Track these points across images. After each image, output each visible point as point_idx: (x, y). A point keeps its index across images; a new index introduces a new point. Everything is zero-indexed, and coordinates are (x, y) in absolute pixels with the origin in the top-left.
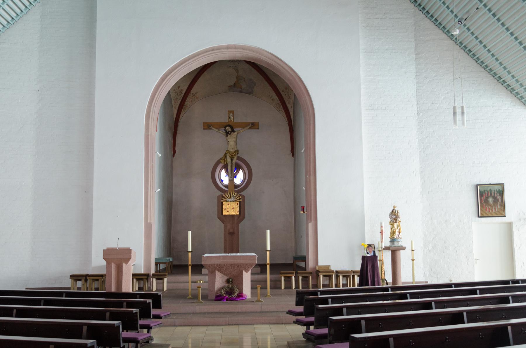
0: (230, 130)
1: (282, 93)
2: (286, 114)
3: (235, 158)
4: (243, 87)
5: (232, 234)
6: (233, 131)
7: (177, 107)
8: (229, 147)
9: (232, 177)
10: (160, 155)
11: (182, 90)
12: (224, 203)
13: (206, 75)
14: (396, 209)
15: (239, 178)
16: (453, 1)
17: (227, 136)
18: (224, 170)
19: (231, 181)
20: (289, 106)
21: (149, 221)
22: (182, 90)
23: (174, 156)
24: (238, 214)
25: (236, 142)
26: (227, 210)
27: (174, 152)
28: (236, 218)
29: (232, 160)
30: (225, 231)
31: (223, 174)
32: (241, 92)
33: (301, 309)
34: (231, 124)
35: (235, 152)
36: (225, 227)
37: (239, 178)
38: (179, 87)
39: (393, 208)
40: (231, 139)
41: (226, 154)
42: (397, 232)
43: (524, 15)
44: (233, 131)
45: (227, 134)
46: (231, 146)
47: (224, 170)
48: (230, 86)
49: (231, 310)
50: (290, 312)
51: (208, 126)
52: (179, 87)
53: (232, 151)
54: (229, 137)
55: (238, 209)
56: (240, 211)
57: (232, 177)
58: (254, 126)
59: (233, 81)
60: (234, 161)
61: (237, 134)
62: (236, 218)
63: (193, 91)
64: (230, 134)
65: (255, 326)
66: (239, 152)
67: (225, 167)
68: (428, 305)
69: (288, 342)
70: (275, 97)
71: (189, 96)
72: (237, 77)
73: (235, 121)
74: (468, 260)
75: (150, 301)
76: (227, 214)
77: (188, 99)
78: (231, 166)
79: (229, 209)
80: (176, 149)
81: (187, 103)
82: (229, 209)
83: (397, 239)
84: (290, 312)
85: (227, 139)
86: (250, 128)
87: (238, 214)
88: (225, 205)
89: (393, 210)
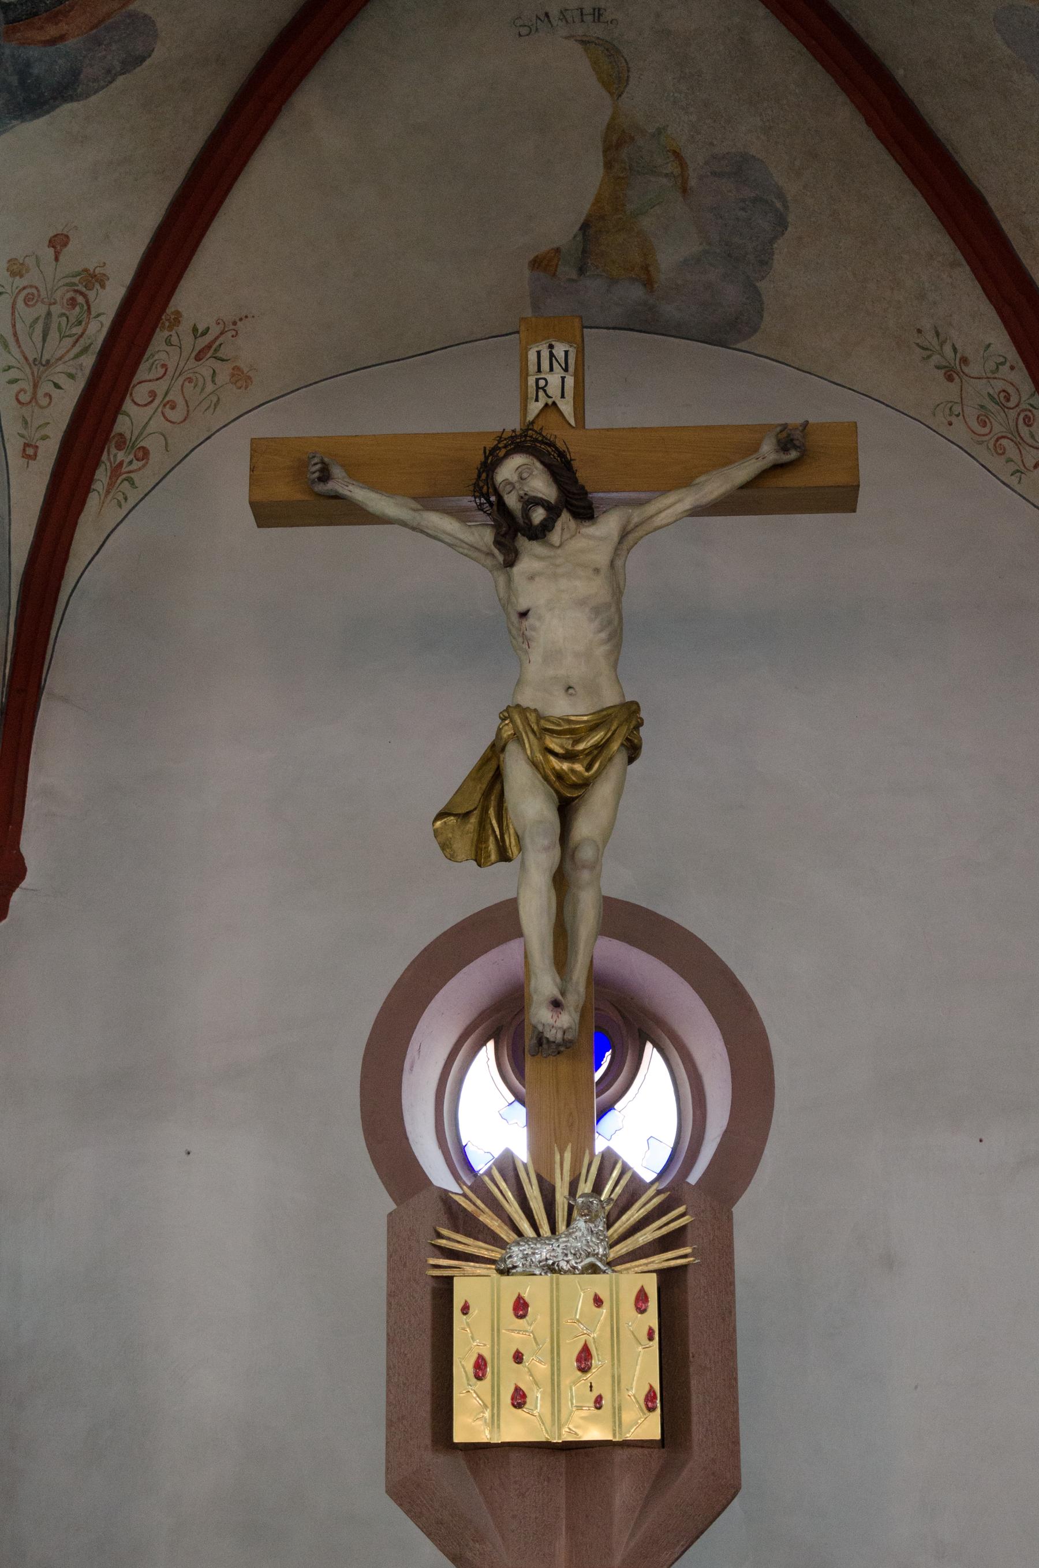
0: (541, 485)
4: (668, 257)
8: (535, 667)
9: (566, 1110)
11: (94, 279)
12: (463, 1290)
15: (643, 1124)
18: (488, 1052)
22: (94, 279)
25: (616, 626)
26: (511, 1377)
28: (624, 1490)
29: (566, 810)
31: (484, 1075)
32: (644, 322)
35: (601, 720)
38: (58, 242)
40: (560, 589)
41: (491, 778)
44: (577, 504)
46: (552, 656)
47: (488, 1052)
49: (65, 601)
51: (305, 493)
52: (58, 242)
53: (561, 707)
54: (525, 565)
55: (643, 1368)
56: (672, 1396)
57: (566, 1110)
59: (562, 198)
62: (624, 1490)
64: (539, 533)
67: (503, 1022)
71: (163, 352)
72: (616, 143)
73: (594, 420)
76: (516, 1428)
81: (135, 416)
87: (648, 1427)
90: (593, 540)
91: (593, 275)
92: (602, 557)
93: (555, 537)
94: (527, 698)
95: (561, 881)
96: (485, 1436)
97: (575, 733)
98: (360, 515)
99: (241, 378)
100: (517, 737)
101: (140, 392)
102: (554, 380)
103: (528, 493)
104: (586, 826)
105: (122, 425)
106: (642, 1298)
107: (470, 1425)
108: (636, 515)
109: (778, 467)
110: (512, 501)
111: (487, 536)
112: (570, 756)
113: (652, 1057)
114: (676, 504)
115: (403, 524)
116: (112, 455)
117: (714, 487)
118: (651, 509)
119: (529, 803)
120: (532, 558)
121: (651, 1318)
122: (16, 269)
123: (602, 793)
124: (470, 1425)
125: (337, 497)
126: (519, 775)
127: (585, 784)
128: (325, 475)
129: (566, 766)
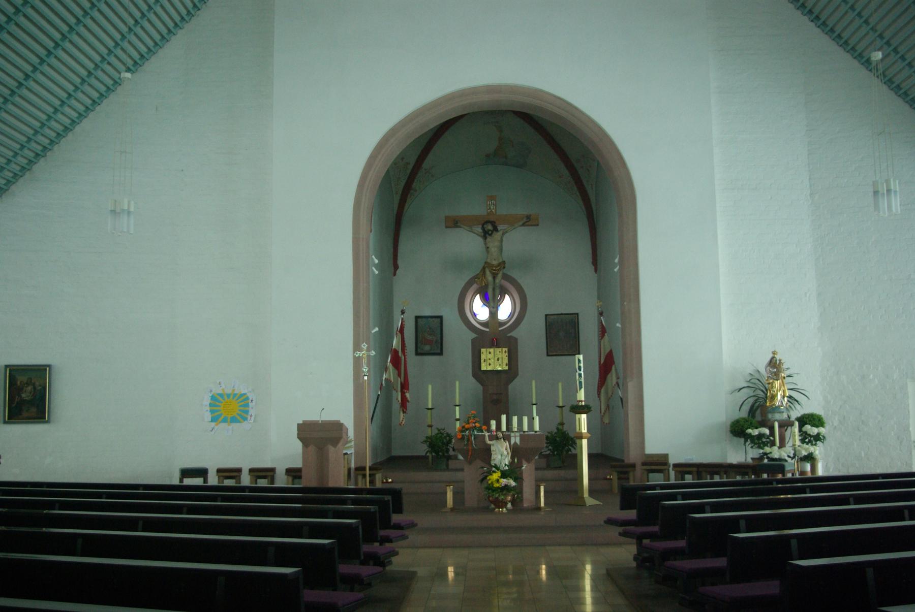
2: (584, 200)
3: (500, 276)
6: (495, 229)
7: (400, 192)
11: (408, 164)
13: (448, 136)
14: (778, 357)
15: (505, 309)
16: (869, 2)
17: (485, 238)
18: (478, 296)
19: (493, 314)
22: (408, 164)
23: (395, 275)
24: (506, 368)
27: (396, 267)
29: (494, 278)
30: (484, 397)
33: (632, 514)
35: (499, 264)
37: (505, 309)
39: (771, 355)
40: (493, 242)
41: (484, 269)
42: (779, 397)
43: (121, 3)
45: (486, 234)
47: (478, 296)
48: (488, 156)
50: (610, 522)
52: (402, 159)
53: (495, 263)
55: (506, 361)
56: (509, 364)
58: (529, 221)
60: (497, 281)
63: (426, 165)
64: (490, 235)
65: (548, 548)
68: (844, 501)
69: (607, 570)
70: (565, 172)
74: (901, 443)
75: (388, 498)
76: (489, 368)
78: (494, 289)
79: (491, 362)
80: (399, 262)
81: (415, 185)
82: (491, 362)
83: (779, 407)
84: (610, 522)
85: (485, 244)
86: (523, 225)
87: (506, 368)
88: (485, 354)
89: (773, 358)
90: (497, 236)
94: (489, 261)
99: (433, 176)
107: (484, 368)
113: (507, 296)
124: (484, 368)
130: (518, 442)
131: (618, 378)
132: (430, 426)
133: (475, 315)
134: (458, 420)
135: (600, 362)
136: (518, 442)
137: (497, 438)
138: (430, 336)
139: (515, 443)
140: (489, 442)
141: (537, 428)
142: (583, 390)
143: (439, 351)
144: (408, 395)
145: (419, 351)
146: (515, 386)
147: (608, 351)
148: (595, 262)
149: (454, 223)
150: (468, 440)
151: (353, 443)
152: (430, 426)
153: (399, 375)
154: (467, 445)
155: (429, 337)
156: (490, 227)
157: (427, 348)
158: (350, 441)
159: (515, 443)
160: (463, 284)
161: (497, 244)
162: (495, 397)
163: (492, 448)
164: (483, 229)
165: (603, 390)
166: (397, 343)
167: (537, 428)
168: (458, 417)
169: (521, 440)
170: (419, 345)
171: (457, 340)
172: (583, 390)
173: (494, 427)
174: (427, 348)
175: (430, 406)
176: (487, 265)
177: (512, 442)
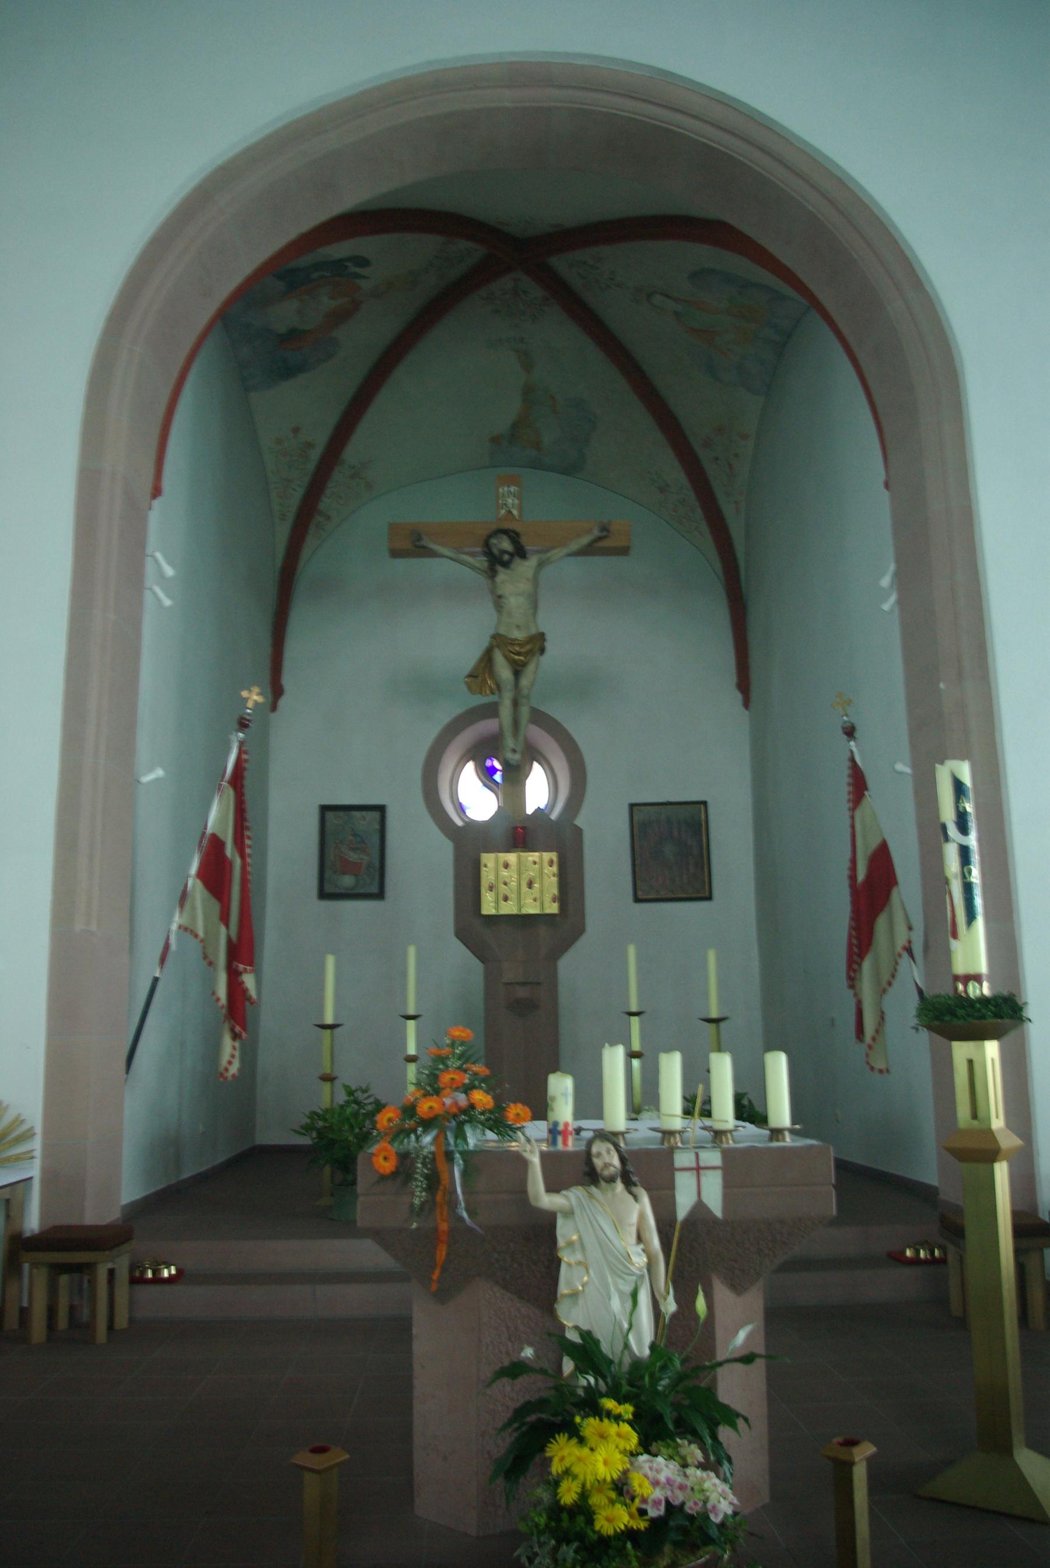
1: (705, 456)
5: (524, 1008)
7: (291, 517)
10: (167, 602)
15: (538, 791)
17: (492, 573)
18: (470, 766)
20: (728, 509)
21: (79, 926)
22: (310, 445)
23: (274, 708)
24: (553, 908)
29: (517, 674)
31: (469, 777)
32: (536, 465)
34: (507, 525)
36: (491, 978)
38: (296, 431)
41: (487, 659)
44: (521, 552)
47: (470, 766)
48: (495, 440)
52: (296, 431)
53: (518, 635)
56: (563, 898)
58: (602, 545)
61: (541, 565)
63: (353, 452)
64: (506, 565)
66: (548, 645)
67: (481, 752)
70: (674, 473)
72: (528, 392)
76: (508, 908)
77: (331, 488)
80: (287, 681)
81: (326, 503)
85: (493, 591)
86: (587, 551)
87: (553, 908)
90: (525, 568)
91: (516, 447)
92: (530, 574)
93: (512, 566)
94: (502, 631)
95: (516, 704)
96: (493, 912)
97: (521, 645)
98: (433, 554)
100: (498, 646)
101: (328, 492)
102: (510, 501)
103: (500, 550)
104: (524, 682)
105: (321, 506)
106: (551, 863)
107: (488, 907)
108: (544, 557)
109: (600, 539)
110: (495, 551)
111: (486, 564)
112: (519, 654)
114: (558, 553)
115: (451, 559)
116: (319, 519)
117: (575, 546)
118: (549, 555)
119: (504, 672)
120: (502, 575)
121: (555, 869)
122: (279, 441)
123: (531, 668)
124: (488, 907)
125: (424, 547)
126: (499, 659)
127: (524, 665)
128: (420, 539)
129: (517, 657)
130: (714, 1200)
131: (910, 928)
132: (328, 1078)
133: (461, 809)
134: (412, 1059)
135: (853, 877)
136: (714, 1200)
137: (592, 1176)
138: (352, 854)
139: (700, 1206)
140: (547, 1201)
141: (781, 1109)
142: (980, 922)
143: (374, 889)
144: (249, 980)
145: (328, 888)
146: (571, 967)
147: (874, 843)
148: (744, 685)
149: (412, 544)
150: (433, 1181)
151: (36, 1144)
152: (328, 1078)
153: (225, 918)
154: (428, 1208)
155: (353, 857)
156: (506, 545)
157: (347, 881)
158: (29, 1135)
159: (700, 1206)
160: (433, 732)
161: (525, 586)
162: (522, 993)
163: (565, 1231)
164: (488, 551)
165: (867, 965)
166: (222, 819)
167: (781, 1109)
168: (412, 1050)
169: (728, 1185)
170: (328, 874)
171: (418, 859)
172: (980, 922)
173: (564, 1111)
174: (347, 881)
175: (329, 1020)
176: (498, 641)
177: (684, 1203)
